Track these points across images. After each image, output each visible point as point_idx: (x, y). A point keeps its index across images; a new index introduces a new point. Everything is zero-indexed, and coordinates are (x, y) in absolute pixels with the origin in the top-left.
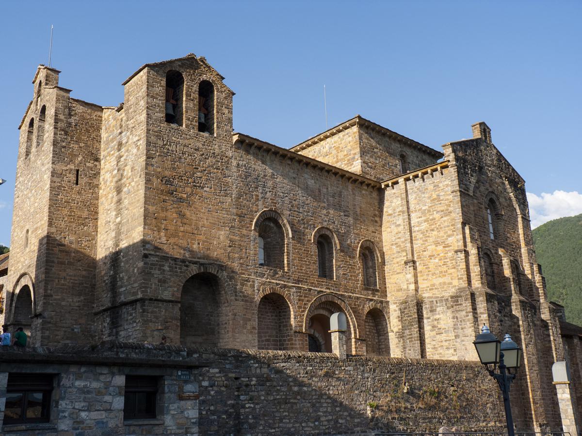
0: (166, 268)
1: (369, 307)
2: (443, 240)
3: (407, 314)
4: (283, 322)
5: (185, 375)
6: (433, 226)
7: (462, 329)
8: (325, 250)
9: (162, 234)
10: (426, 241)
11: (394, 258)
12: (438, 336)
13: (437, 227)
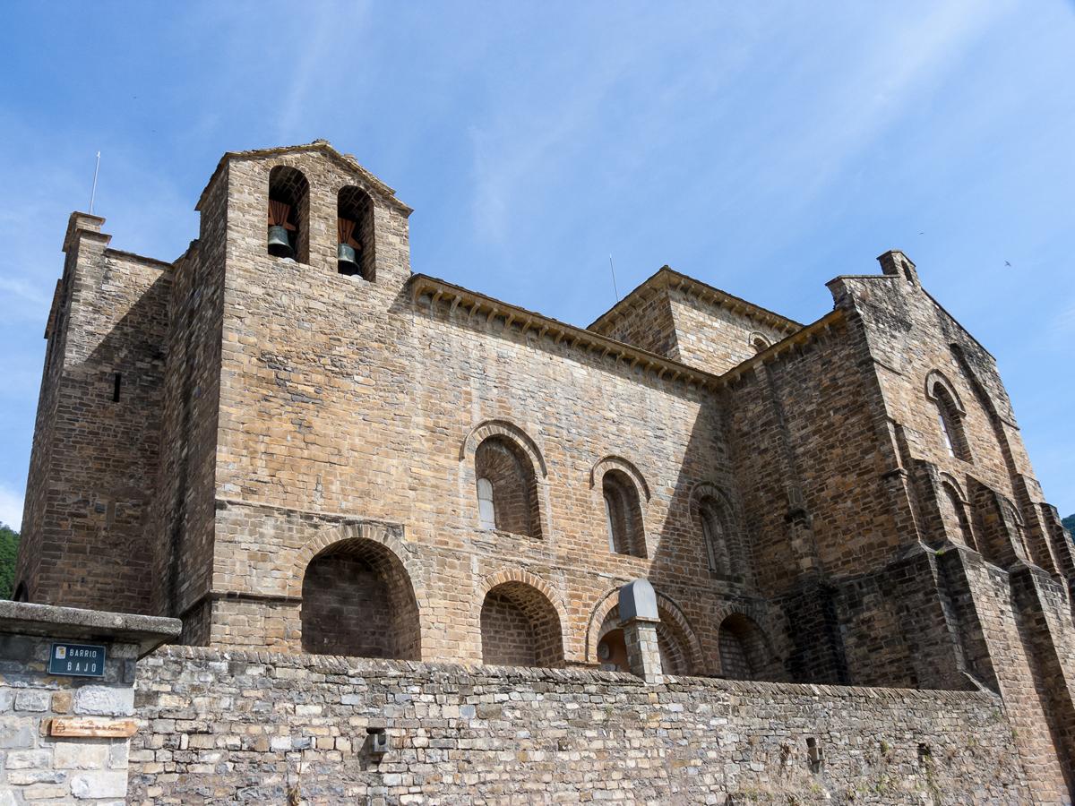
0: (268, 530)
1: (725, 611)
2: (855, 461)
3: (803, 618)
4: (543, 645)
5: (83, 660)
6: (831, 440)
7: (922, 629)
8: (622, 503)
9: (260, 463)
10: (823, 469)
11: (763, 515)
12: (874, 656)
13: (840, 438)
